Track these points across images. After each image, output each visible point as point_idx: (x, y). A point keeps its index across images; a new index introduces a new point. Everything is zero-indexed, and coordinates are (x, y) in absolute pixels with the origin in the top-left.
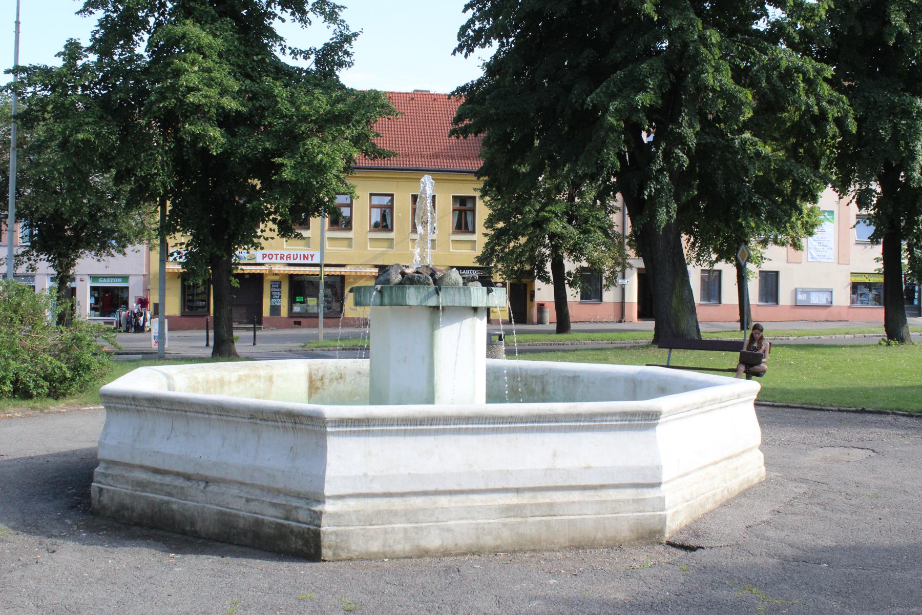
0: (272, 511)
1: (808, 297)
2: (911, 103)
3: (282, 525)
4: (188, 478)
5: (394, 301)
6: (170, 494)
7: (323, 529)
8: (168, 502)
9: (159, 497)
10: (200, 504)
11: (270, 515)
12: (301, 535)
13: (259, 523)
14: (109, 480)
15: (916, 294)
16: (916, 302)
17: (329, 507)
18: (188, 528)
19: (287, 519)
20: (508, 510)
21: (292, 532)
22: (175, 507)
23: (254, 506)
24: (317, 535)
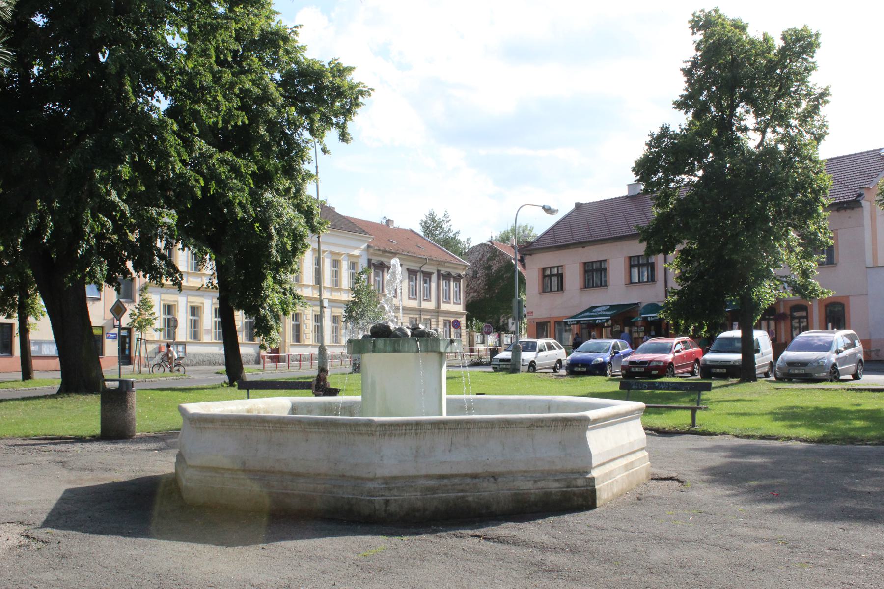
0: (556, 485)
1: (40, 349)
2: (262, 195)
3: (566, 492)
4: (475, 476)
5: (430, 349)
6: (462, 491)
7: (597, 487)
8: (463, 497)
9: (453, 495)
10: (488, 491)
11: (554, 486)
12: (582, 495)
13: (547, 494)
14: (395, 492)
15: (127, 345)
16: (127, 352)
17: (594, 473)
18: (484, 512)
19: (568, 487)
20: (627, 467)
21: (574, 494)
22: (470, 499)
23: (541, 484)
24: (593, 492)
